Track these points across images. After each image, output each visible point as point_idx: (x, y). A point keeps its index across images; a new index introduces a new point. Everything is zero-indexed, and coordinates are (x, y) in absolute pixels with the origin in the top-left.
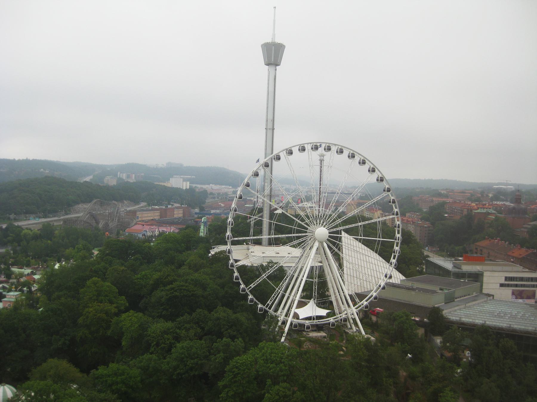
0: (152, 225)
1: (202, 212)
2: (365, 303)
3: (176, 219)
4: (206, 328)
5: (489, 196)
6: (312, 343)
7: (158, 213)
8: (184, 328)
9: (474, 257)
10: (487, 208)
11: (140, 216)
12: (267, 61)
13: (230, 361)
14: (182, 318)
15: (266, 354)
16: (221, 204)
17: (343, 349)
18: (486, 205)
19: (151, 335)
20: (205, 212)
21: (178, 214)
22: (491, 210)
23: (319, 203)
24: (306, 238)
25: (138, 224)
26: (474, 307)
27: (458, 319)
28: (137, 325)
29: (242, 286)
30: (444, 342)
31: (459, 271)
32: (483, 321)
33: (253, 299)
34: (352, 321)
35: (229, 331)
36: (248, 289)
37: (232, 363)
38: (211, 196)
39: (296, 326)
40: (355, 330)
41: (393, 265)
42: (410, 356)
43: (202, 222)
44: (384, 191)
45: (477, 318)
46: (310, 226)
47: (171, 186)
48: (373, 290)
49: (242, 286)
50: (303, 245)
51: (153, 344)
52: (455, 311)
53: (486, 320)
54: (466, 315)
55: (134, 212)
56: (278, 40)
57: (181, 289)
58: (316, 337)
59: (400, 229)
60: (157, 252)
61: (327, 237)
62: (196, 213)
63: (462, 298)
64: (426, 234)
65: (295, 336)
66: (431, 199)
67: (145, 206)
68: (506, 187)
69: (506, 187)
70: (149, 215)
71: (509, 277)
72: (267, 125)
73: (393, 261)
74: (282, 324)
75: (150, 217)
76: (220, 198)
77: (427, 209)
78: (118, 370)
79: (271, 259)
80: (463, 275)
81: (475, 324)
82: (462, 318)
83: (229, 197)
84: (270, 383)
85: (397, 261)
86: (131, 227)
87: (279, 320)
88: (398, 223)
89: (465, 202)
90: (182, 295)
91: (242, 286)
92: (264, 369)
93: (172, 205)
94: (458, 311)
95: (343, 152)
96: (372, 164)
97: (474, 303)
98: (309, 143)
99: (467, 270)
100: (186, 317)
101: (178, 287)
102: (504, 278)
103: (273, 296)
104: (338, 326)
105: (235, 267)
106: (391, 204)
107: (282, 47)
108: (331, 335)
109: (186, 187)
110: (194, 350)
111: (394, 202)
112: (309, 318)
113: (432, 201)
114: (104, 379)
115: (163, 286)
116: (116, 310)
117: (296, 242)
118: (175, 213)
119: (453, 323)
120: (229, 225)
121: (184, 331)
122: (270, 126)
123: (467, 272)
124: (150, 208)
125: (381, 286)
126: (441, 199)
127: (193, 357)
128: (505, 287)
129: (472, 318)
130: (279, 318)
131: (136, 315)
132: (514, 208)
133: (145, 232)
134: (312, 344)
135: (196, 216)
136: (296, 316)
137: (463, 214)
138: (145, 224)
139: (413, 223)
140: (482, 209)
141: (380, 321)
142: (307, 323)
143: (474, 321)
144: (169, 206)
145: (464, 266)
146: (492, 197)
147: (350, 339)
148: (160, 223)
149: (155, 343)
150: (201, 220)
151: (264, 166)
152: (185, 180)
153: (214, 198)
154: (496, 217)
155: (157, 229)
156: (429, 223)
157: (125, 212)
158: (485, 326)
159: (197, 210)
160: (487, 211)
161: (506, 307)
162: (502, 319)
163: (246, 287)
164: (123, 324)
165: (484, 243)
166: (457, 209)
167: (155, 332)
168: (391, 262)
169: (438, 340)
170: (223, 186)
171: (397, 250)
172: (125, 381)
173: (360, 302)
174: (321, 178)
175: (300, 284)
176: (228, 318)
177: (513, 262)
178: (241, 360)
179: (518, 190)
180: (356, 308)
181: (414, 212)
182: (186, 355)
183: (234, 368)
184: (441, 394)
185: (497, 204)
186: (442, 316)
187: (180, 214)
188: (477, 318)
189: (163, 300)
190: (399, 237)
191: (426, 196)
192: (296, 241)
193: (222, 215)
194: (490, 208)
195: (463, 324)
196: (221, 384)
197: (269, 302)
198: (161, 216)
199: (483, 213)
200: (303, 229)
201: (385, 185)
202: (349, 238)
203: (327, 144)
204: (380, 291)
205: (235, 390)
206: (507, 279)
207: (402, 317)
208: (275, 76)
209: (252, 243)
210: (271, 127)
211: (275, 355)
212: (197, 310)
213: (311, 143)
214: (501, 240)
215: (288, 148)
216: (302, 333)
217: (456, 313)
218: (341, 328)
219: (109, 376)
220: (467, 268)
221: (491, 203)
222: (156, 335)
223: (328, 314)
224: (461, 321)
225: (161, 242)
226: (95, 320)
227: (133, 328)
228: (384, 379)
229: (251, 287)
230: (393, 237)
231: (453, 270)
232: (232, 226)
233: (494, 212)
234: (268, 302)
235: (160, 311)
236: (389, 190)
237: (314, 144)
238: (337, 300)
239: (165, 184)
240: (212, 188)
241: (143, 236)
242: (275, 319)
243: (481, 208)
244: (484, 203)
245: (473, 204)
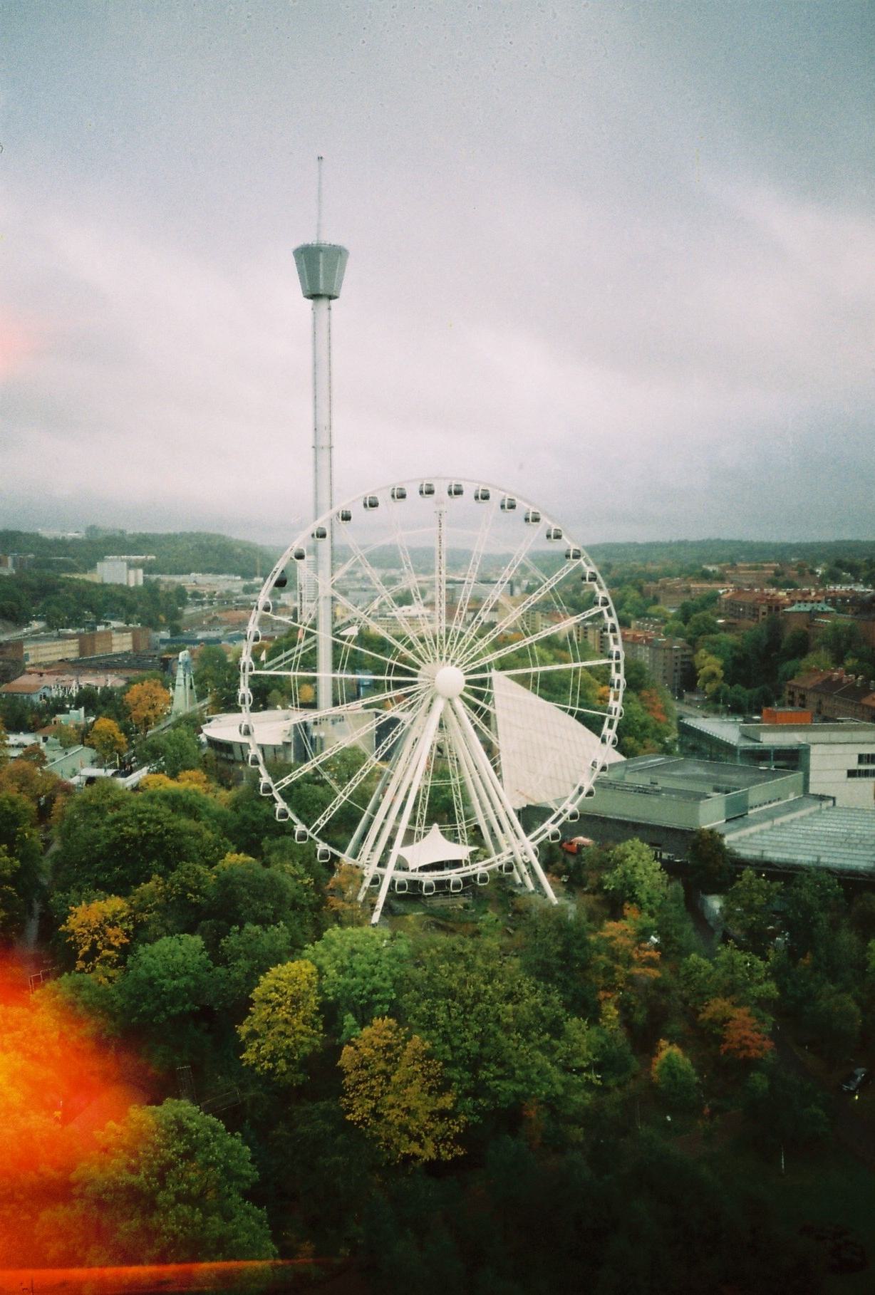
0: (60, 673)
1: (175, 638)
2: (550, 827)
3: (116, 655)
5: (818, 573)
9: (787, 712)
10: (812, 602)
11: (31, 653)
13: (262, 978)
18: (810, 593)
22: (822, 605)
27: (757, 853)
29: (300, 827)
32: (814, 856)
34: (524, 869)
37: (267, 981)
39: (402, 887)
41: (609, 742)
48: (566, 798)
49: (280, 804)
61: (464, 685)
62: (163, 641)
67: (43, 630)
70: (54, 650)
71: (868, 755)
72: (316, 438)
73: (610, 733)
74: (371, 884)
80: (760, 755)
81: (795, 865)
82: (767, 850)
83: (238, 602)
85: (618, 732)
87: (366, 875)
90: (144, 832)
91: (300, 827)
93: (107, 624)
94: (757, 837)
96: (531, 504)
99: (774, 744)
109: (136, 582)
113: (688, 591)
118: (115, 642)
120: (244, 671)
124: (55, 633)
130: (365, 873)
135: (163, 647)
136: (402, 866)
138: (46, 671)
139: (648, 641)
140: (802, 605)
143: (794, 857)
144: (100, 628)
145: (765, 734)
150: (175, 656)
155: (74, 682)
159: (165, 634)
161: (863, 823)
171: (616, 709)
175: (406, 797)
180: (533, 840)
181: (649, 617)
185: (834, 592)
190: (619, 681)
194: (819, 602)
195: (769, 864)
196: (243, 1030)
198: (82, 651)
199: (803, 612)
200: (406, 671)
204: (583, 800)
206: (861, 759)
209: (296, 706)
217: (754, 841)
220: (771, 739)
221: (821, 590)
224: (764, 859)
231: (742, 745)
233: (830, 609)
238: (488, 823)
239: (88, 577)
240: (195, 582)
242: (355, 875)
243: (799, 602)
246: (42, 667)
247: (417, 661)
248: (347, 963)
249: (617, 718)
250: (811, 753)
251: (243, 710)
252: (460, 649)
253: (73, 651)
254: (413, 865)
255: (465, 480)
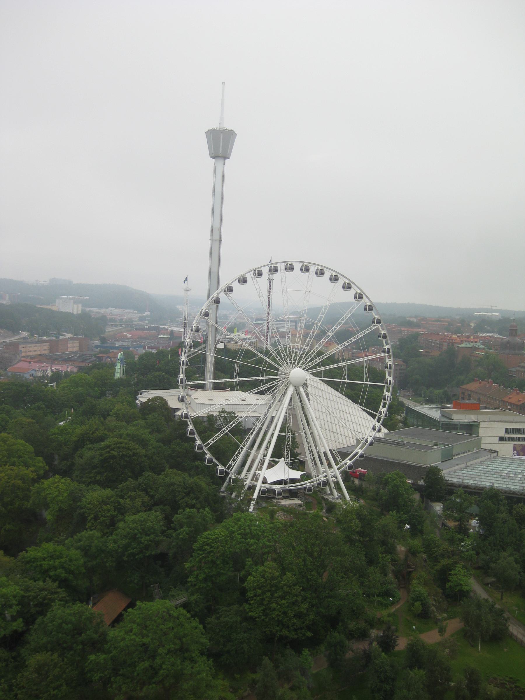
4: (157, 496)
6: (285, 513)
7: (46, 345)
8: (129, 497)
10: (472, 342)
11: (23, 350)
12: (213, 152)
14: (125, 484)
15: (243, 526)
16: (127, 334)
17: (324, 519)
19: (87, 506)
20: (108, 345)
21: (73, 347)
22: (478, 344)
23: (267, 334)
24: (278, 381)
25: (22, 361)
26: (477, 466)
27: (460, 480)
28: (65, 494)
29: (199, 442)
30: (445, 509)
31: (449, 422)
32: (490, 482)
33: (211, 459)
34: (333, 485)
35: (186, 499)
36: (206, 446)
37: (200, 540)
38: (112, 323)
40: (337, 496)
42: (409, 527)
43: (119, 359)
44: (373, 322)
45: (482, 480)
46: (281, 366)
47: (57, 310)
50: (273, 391)
51: (89, 518)
52: (456, 470)
53: (494, 481)
54: (469, 476)
55: (15, 346)
56: (227, 126)
57: (119, 448)
58: (290, 505)
59: (392, 370)
60: (64, 398)
62: (96, 347)
63: (461, 455)
64: (396, 374)
65: (264, 504)
66: (399, 329)
68: (490, 314)
69: (490, 314)
70: (36, 348)
72: (212, 235)
75: (36, 351)
76: (124, 325)
77: (394, 342)
78: (55, 551)
79: (224, 408)
83: (136, 325)
84: (251, 562)
86: (14, 365)
88: (389, 362)
89: (444, 333)
91: (199, 442)
92: (242, 545)
94: (459, 471)
95: (324, 273)
97: (476, 461)
98: (283, 262)
100: (131, 482)
101: (116, 445)
102: (504, 430)
103: (236, 454)
104: (315, 492)
105: (190, 419)
106: (382, 339)
107: (232, 134)
108: (306, 502)
110: (149, 524)
111: (385, 337)
112: (280, 482)
114: (39, 563)
115: (90, 443)
116: (34, 475)
117: (263, 387)
118: (69, 345)
119: (453, 485)
120: (183, 365)
121: (128, 501)
122: (216, 237)
123: (459, 422)
125: (369, 442)
126: (412, 330)
127: (149, 532)
128: (505, 441)
129: (477, 479)
131: (63, 480)
132: (508, 342)
133: (33, 372)
134: (285, 514)
136: (265, 481)
137: (442, 348)
140: (467, 343)
141: (365, 485)
142: (278, 488)
143: (479, 483)
144: (61, 337)
145: (455, 415)
146: (474, 327)
147: (331, 508)
148: (51, 359)
149: (92, 516)
151: (226, 291)
152: (76, 302)
153: (115, 326)
154: (487, 353)
155: (49, 368)
156: (400, 361)
157: (4, 345)
158: (494, 489)
160: (474, 345)
162: (513, 481)
163: (204, 443)
164: (48, 492)
165: (473, 386)
166: (434, 343)
167: (92, 502)
168: (380, 411)
169: (438, 507)
170: (126, 311)
171: (388, 396)
172: (65, 565)
173: (343, 461)
174: (269, 302)
176: (184, 483)
177: (510, 409)
178: (212, 536)
179: (514, 320)
182: (140, 530)
183: (204, 546)
184: (452, 572)
185: (484, 337)
186: (441, 477)
187: (75, 347)
188: (482, 480)
189: (96, 461)
190: (390, 381)
191: (392, 325)
192: (265, 385)
193: (131, 349)
194: (476, 342)
195: (466, 487)
197: (230, 462)
198: (51, 351)
200: (273, 370)
201: (374, 315)
202: (315, 380)
203: (305, 264)
204: (367, 447)
205: (207, 572)
206: (507, 431)
207: (395, 480)
208: (223, 172)
210: (218, 238)
211: (255, 528)
212: (144, 474)
213: (285, 262)
214: (494, 382)
215: (257, 268)
216: (272, 501)
218: (318, 494)
219: (44, 559)
220: (460, 417)
222: (93, 506)
223: (302, 476)
225: (68, 385)
226: (8, 488)
227: (61, 498)
228: (380, 556)
229: (209, 444)
230: (382, 379)
232: (186, 367)
233: (482, 346)
234: (230, 463)
235: (92, 475)
236: (379, 322)
237: (289, 263)
240: (111, 313)
241: (30, 377)
244: (468, 334)
245: (454, 336)
246: (29, 358)
247: (277, 366)
248: (248, 531)
249: (388, 402)
250: (480, 426)
251: (180, 387)
252: (306, 360)
253: (46, 350)
254: (269, 481)
255: (326, 268)
